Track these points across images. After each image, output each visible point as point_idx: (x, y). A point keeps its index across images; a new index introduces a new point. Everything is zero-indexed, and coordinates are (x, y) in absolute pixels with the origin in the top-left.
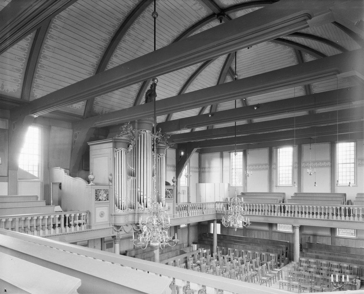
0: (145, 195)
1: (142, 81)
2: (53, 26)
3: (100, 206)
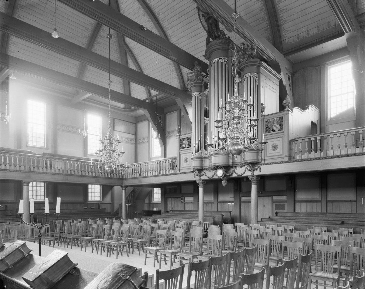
3: (272, 138)
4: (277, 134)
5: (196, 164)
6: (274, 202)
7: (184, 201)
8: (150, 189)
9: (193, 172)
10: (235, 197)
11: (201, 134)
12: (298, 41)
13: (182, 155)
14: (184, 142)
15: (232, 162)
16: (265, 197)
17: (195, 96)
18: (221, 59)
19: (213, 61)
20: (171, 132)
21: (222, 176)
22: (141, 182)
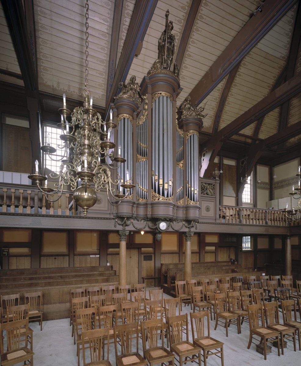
3: (207, 200)
4: (206, 198)
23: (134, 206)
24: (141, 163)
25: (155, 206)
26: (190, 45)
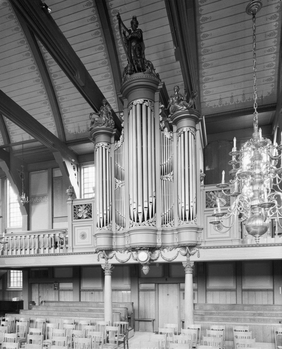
0: (140, 206)
1: (43, 144)
2: (64, 111)
5: (103, 242)
6: (181, 291)
7: (59, 287)
8: (6, 271)
9: (96, 252)
10: (132, 284)
11: (110, 201)
12: (219, 106)
13: (76, 228)
14: (80, 210)
15: (160, 242)
16: (169, 285)
17: (102, 148)
18: (147, 101)
19: (135, 102)
20: (39, 197)
21: (146, 260)
22: (5, 264)
23: (113, 237)
24: (117, 191)
25: (181, 231)
26: (54, 80)
